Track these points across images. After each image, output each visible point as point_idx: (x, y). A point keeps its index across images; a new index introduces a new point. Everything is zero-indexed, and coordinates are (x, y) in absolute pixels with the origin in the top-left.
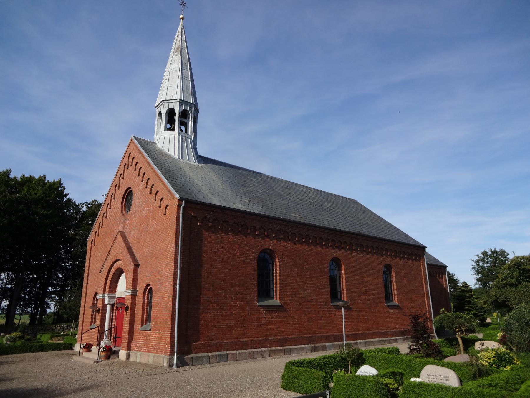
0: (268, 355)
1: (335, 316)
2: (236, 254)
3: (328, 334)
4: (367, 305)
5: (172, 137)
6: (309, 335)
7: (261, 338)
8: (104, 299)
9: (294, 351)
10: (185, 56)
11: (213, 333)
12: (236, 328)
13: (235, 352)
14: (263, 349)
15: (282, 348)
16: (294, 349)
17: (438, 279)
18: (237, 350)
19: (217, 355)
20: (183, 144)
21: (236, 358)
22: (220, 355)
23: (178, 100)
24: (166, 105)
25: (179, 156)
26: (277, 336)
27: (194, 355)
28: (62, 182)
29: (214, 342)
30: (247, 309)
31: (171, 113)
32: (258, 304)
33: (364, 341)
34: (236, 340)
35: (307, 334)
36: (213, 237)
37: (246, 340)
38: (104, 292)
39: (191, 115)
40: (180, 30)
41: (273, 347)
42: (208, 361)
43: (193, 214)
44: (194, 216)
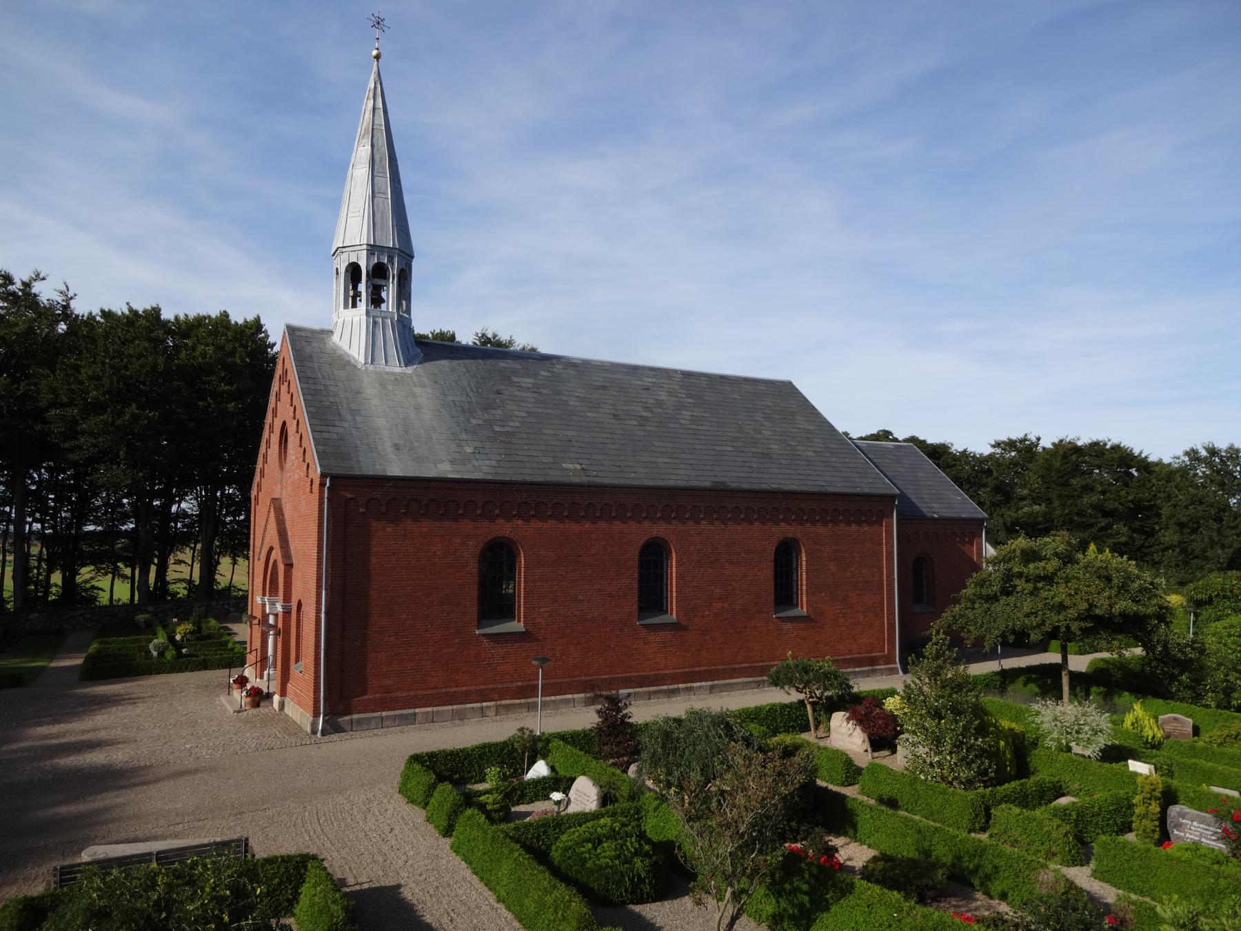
0: (494, 713)
1: (645, 643)
2: (435, 552)
3: (627, 675)
4: (725, 619)
5: (356, 319)
6: (583, 678)
7: (482, 687)
8: (264, 605)
9: (549, 706)
10: (380, 145)
11: (391, 682)
12: (433, 673)
13: (430, 709)
14: (485, 704)
15: (523, 701)
16: (548, 701)
17: (959, 545)
18: (436, 706)
19: (395, 716)
20: (377, 332)
21: (431, 719)
22: (402, 715)
23: (365, 247)
24: (344, 256)
25: (366, 359)
26: (516, 681)
27: (355, 716)
28: (262, 322)
29: (392, 695)
30: (457, 641)
31: (354, 272)
32: (477, 632)
33: (709, 683)
34: (433, 692)
35: (580, 676)
36: (389, 530)
37: (453, 690)
38: (264, 595)
39: (393, 271)
40: (372, 85)
41: (506, 699)
42: (380, 724)
43: (349, 496)
44: (352, 499)
